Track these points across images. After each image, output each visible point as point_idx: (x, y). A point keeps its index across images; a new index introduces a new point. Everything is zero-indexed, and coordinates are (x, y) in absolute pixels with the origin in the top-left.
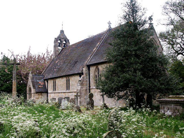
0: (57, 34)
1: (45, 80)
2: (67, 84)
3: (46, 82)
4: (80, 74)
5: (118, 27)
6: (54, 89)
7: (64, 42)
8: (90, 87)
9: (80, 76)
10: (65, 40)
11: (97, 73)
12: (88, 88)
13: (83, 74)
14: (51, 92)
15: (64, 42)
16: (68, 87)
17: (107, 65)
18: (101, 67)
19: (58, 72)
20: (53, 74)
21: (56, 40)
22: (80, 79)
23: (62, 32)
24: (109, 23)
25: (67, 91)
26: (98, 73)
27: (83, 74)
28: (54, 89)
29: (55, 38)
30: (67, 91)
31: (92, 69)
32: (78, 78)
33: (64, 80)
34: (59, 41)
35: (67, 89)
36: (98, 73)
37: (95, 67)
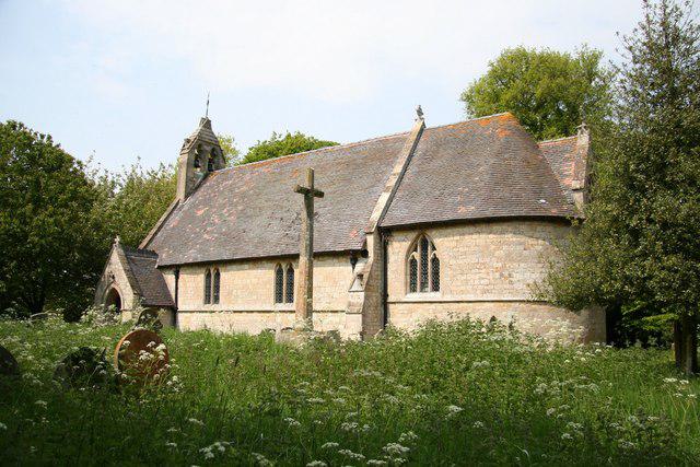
0: (193, 129)
4: (355, 256)
8: (385, 295)
11: (417, 255)
12: (380, 300)
13: (364, 253)
23: (207, 124)
29: (188, 141)
31: (399, 249)
32: (344, 272)
37: (412, 235)
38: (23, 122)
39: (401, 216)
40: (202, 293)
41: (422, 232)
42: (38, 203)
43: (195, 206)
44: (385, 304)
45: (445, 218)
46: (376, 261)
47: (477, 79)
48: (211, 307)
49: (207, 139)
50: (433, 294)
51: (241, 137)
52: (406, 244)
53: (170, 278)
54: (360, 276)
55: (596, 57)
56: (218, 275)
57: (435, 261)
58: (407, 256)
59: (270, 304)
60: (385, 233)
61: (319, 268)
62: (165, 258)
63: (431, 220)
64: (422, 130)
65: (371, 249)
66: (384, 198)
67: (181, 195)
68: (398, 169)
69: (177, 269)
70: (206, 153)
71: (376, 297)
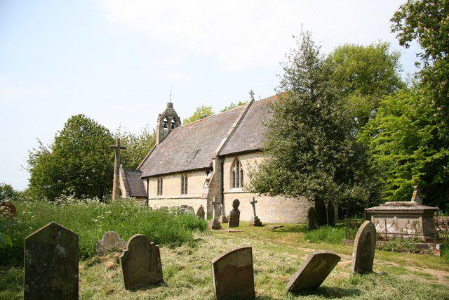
0: (163, 109)
1: (143, 178)
2: (234, 179)
3: (145, 183)
4: (208, 170)
5: (108, 137)
6: (160, 191)
7: (173, 121)
8: (222, 190)
9: (208, 173)
10: (174, 118)
11: (235, 169)
12: (220, 192)
13: (211, 169)
14: (153, 198)
15: (173, 121)
16: (184, 189)
17: (260, 160)
18: (245, 162)
19: (165, 166)
20: (157, 170)
21: (162, 117)
22: (208, 178)
23: (171, 105)
24: (252, 93)
25: (183, 196)
26: (238, 169)
27: (211, 169)
28: (160, 191)
29: (160, 115)
30: (160, 197)
31: (228, 165)
32: (203, 177)
33: (177, 181)
34: (165, 120)
35: (182, 193)
36: (238, 169)
37: (233, 159)
38: (80, 113)
39: (230, 149)
40: (156, 190)
41: (236, 155)
42: (88, 150)
43: (161, 147)
44: (223, 194)
45: (244, 150)
46: (217, 172)
47: (291, 66)
48: (160, 197)
49: (170, 113)
50: (238, 189)
51: (184, 113)
52: (231, 163)
53: (145, 183)
54: (208, 180)
55: (385, 47)
56: (187, 179)
57: (242, 171)
58: (231, 170)
59: (179, 195)
60: (222, 158)
61: (193, 177)
62: (144, 174)
63: (238, 151)
64: (251, 103)
65: (214, 167)
66: (225, 139)
67: (157, 142)
68: (234, 125)
69: (148, 178)
70: (170, 120)
71: (217, 190)
